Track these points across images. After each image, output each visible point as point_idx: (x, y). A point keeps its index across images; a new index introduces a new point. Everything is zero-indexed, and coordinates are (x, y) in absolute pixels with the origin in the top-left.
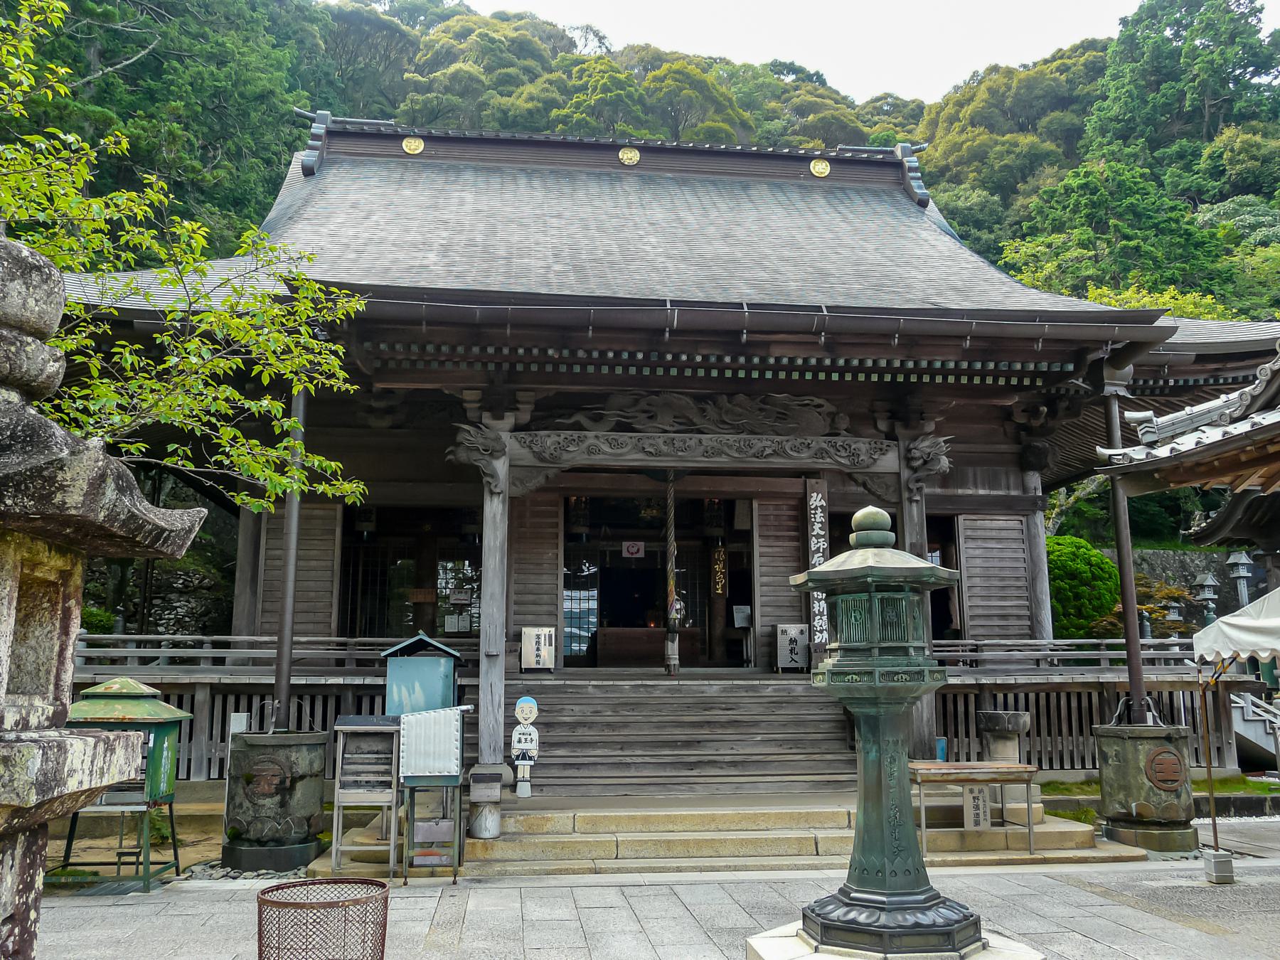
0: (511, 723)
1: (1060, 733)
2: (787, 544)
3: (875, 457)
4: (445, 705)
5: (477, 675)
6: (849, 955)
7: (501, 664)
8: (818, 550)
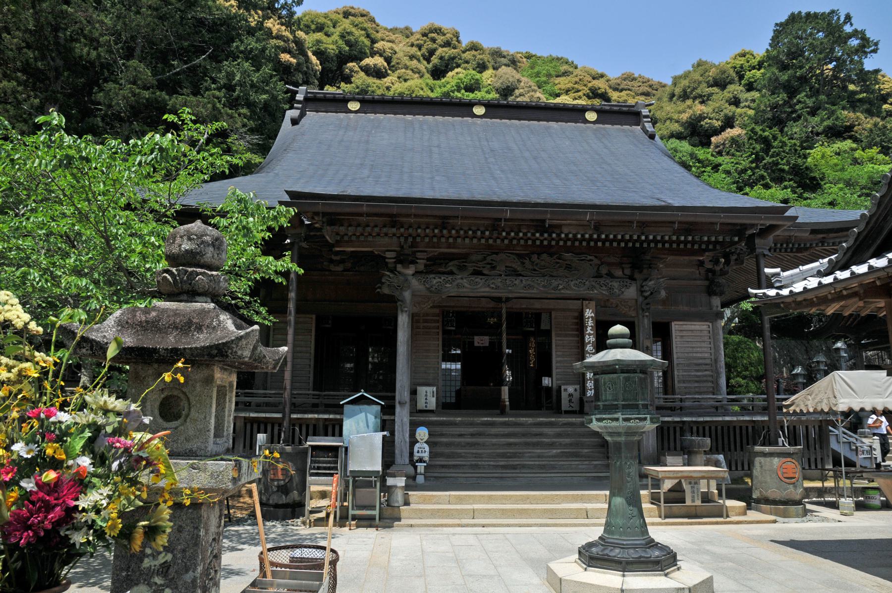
0: (413, 442)
1: (730, 450)
2: (571, 338)
3: (623, 290)
4: (376, 431)
5: (394, 414)
6: (604, 573)
7: (407, 406)
8: (589, 343)
